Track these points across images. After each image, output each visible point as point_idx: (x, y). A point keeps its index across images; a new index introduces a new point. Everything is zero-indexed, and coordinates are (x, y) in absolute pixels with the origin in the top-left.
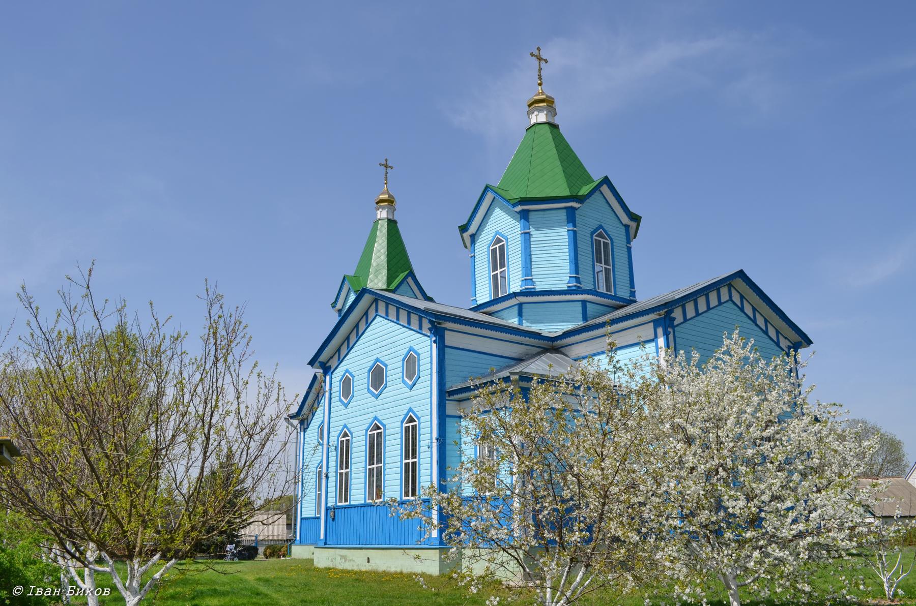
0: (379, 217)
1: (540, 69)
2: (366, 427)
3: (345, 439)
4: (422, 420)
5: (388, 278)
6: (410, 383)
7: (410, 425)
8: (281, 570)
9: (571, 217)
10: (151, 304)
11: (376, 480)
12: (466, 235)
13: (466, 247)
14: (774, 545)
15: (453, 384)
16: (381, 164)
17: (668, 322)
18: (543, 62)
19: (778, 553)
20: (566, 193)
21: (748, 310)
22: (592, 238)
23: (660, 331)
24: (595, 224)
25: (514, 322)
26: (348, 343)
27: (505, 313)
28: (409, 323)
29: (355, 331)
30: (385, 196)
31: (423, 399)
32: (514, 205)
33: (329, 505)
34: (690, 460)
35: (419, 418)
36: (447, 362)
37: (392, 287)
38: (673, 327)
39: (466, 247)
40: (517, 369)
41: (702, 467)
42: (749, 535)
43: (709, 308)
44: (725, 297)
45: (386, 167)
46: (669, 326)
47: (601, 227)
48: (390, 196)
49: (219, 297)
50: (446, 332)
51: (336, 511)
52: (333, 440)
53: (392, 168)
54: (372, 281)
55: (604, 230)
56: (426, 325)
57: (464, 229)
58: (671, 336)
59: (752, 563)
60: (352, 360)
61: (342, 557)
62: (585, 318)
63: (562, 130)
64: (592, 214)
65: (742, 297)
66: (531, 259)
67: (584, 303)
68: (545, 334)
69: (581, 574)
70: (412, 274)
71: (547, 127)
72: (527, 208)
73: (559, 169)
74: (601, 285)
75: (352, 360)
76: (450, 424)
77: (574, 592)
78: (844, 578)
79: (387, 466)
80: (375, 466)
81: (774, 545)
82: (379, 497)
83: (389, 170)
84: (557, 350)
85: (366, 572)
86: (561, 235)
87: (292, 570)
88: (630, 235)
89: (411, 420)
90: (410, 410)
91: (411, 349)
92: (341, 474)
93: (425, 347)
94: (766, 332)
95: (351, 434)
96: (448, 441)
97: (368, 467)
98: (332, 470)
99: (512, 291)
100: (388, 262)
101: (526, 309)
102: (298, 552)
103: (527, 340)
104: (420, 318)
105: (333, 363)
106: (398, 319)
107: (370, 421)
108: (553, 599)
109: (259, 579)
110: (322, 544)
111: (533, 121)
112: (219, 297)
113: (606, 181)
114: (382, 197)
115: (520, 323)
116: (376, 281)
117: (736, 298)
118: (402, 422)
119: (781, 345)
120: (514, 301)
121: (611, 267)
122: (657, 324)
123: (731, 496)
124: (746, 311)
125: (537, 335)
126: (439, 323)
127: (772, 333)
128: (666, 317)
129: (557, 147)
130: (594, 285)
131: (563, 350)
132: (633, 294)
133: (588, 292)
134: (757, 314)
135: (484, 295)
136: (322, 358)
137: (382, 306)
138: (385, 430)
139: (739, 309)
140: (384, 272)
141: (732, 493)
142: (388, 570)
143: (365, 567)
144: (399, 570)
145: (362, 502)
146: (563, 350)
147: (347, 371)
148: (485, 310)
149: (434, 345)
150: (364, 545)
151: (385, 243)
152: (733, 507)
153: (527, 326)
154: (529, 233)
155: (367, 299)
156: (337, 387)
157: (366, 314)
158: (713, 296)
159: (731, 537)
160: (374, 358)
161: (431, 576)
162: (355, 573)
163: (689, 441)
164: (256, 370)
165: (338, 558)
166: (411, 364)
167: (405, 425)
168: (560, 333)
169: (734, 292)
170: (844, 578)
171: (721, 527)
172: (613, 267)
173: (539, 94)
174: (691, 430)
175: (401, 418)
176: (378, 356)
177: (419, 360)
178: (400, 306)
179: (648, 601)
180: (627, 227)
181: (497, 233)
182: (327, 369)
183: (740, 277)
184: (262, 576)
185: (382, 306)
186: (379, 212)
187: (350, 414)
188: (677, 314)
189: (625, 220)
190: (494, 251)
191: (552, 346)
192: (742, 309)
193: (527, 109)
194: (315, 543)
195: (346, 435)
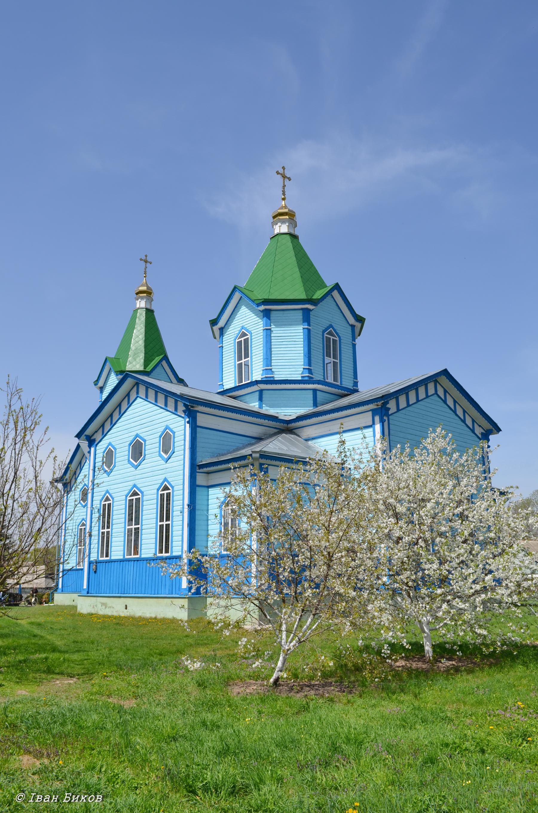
0: (138, 306)
1: (284, 186)
2: (126, 493)
3: (107, 503)
4: (175, 488)
5: (145, 361)
6: (166, 456)
8: (48, 615)
9: (307, 316)
11: (134, 539)
12: (216, 328)
13: (215, 338)
14: (457, 599)
15: (203, 459)
16: (141, 260)
17: (384, 412)
18: (287, 180)
19: (461, 606)
20: (303, 296)
21: (450, 402)
22: (323, 335)
23: (377, 418)
24: (326, 324)
25: (254, 405)
26: (110, 421)
27: (247, 398)
28: (166, 405)
30: (144, 288)
31: (177, 470)
32: (258, 305)
33: (91, 559)
34: (397, 533)
35: (173, 487)
36: (198, 440)
37: (149, 369)
38: (388, 416)
39: (215, 338)
41: (407, 538)
43: (418, 400)
44: (431, 391)
45: (146, 262)
46: (385, 415)
47: (331, 326)
48: (148, 288)
49: (19, 391)
50: (198, 414)
51: (98, 565)
52: (96, 503)
53: (151, 263)
54: (130, 363)
55: (333, 328)
56: (181, 407)
57: (214, 323)
58: (386, 424)
59: (441, 613)
60: (115, 435)
61: (103, 604)
62: (315, 404)
63: (301, 240)
64: (324, 315)
65: (445, 391)
66: (271, 351)
67: (315, 391)
68: (281, 417)
69: (310, 620)
70: (166, 358)
71: (288, 237)
73: (298, 275)
75: (115, 435)
77: (303, 636)
78: (511, 624)
79: (144, 527)
80: (133, 527)
81: (457, 599)
82: (167, 551)
83: (148, 264)
84: (290, 431)
85: (125, 617)
87: (59, 615)
88: (355, 333)
90: (166, 480)
91: (167, 428)
92: (103, 533)
93: (180, 427)
94: (464, 421)
95: (113, 498)
96: (197, 507)
97: (127, 527)
100: (146, 347)
101: (265, 394)
102: (60, 599)
103: (266, 422)
106: (156, 401)
107: (130, 487)
108: (287, 640)
109: (32, 623)
110: (85, 593)
111: (277, 231)
112: (19, 391)
113: (337, 287)
114: (142, 288)
115: (261, 407)
116: (134, 363)
117: (441, 392)
118: (158, 490)
119: (476, 432)
120: (256, 388)
121: (338, 361)
122: (374, 412)
123: (428, 560)
124: (448, 403)
125: (274, 418)
126: (192, 407)
127: (469, 422)
128: (382, 407)
129: (296, 255)
130: (324, 376)
132: (356, 384)
133: (318, 382)
135: (230, 382)
136: (88, 432)
138: (143, 496)
140: (142, 356)
141: (430, 557)
142: (143, 615)
143: (124, 613)
144: (153, 616)
145: (122, 557)
147: (110, 444)
148: (230, 394)
149: (188, 425)
150: (122, 593)
151: (143, 330)
152: (428, 570)
154: (270, 329)
155: (129, 382)
157: (128, 395)
158: (422, 390)
159: (426, 593)
160: (135, 433)
162: (115, 618)
163: (397, 516)
164: (53, 455)
165: (99, 605)
166: (167, 442)
167: (160, 493)
168: (293, 417)
169: (439, 387)
170: (511, 624)
171: (418, 585)
172: (340, 361)
173: (282, 208)
174: (401, 509)
175: (157, 486)
176: (138, 432)
177: (174, 437)
178: (158, 390)
179: (361, 641)
180: (353, 326)
181: (243, 328)
182: (91, 442)
183: (444, 375)
184: (33, 620)
186: (138, 302)
187: (116, 483)
188: (392, 405)
189: (352, 320)
190: (240, 343)
191: (287, 427)
192: (445, 402)
193: (272, 220)
194: (77, 590)
195: (107, 499)
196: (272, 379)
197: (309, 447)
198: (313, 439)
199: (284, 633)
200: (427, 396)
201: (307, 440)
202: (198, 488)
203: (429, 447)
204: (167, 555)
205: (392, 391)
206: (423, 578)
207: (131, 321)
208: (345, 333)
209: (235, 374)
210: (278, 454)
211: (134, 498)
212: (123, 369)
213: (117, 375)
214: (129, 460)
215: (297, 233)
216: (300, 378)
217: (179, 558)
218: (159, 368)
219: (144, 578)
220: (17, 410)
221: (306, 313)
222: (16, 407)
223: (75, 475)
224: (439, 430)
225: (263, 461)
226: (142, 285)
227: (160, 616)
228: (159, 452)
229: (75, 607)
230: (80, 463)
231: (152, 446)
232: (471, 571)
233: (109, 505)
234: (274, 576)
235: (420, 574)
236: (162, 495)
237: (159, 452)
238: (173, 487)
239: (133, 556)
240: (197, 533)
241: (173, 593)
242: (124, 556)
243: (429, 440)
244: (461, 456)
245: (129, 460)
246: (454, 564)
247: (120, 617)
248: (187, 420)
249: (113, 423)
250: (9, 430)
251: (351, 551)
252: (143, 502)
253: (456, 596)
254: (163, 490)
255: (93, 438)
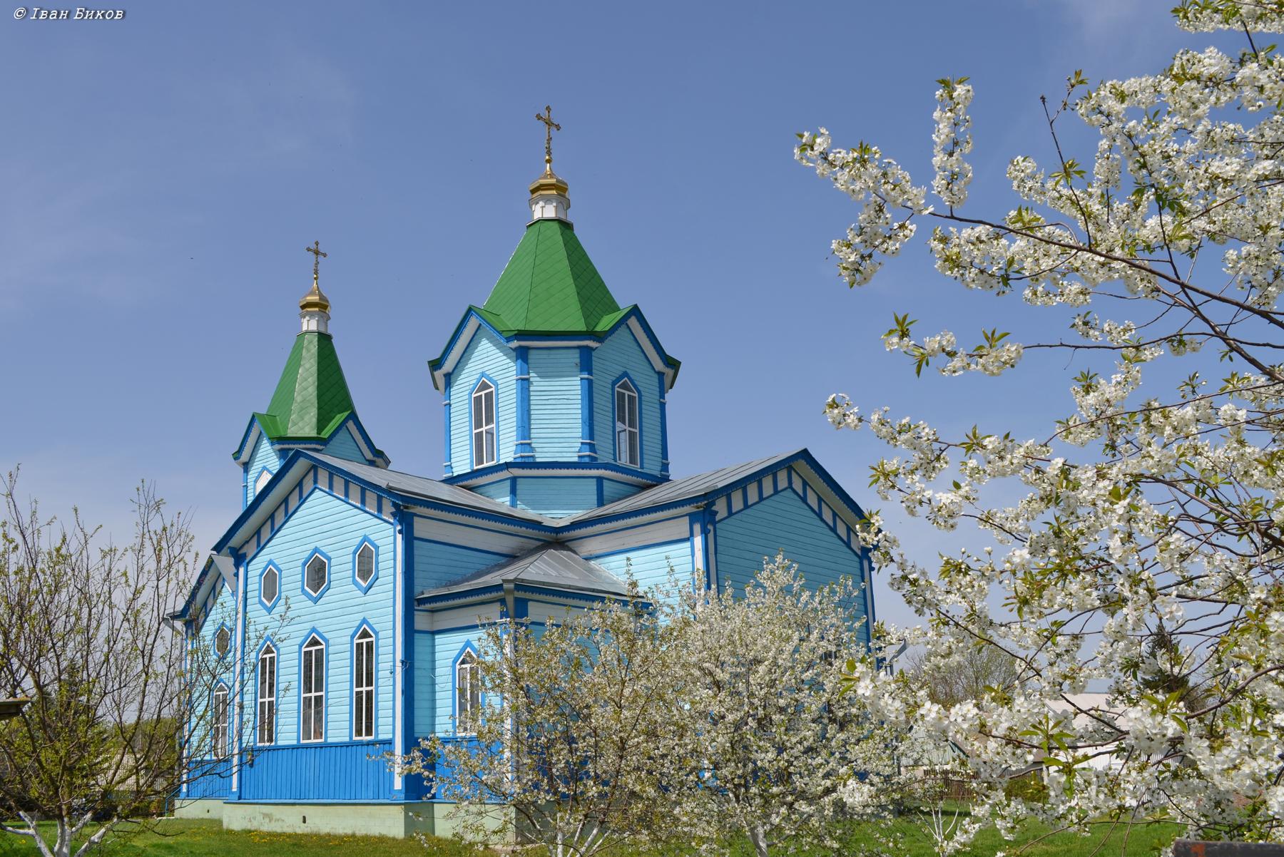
0: (305, 328)
5: (319, 421)
6: (364, 585)
7: (364, 641)
9: (586, 364)
10: (76, 510)
11: (314, 710)
12: (439, 374)
13: (437, 388)
16: (309, 249)
20: (581, 326)
21: (812, 500)
22: (613, 389)
23: (697, 528)
24: (618, 371)
25: (502, 502)
29: (283, 507)
30: (315, 298)
31: (383, 606)
32: (508, 340)
35: (376, 633)
36: (416, 559)
37: (326, 434)
38: (714, 523)
39: (437, 388)
40: (511, 573)
42: (775, 790)
43: (761, 499)
44: (783, 483)
45: (317, 253)
47: (625, 374)
50: (416, 519)
53: (325, 255)
54: (295, 424)
56: (388, 507)
57: (435, 365)
58: (711, 536)
61: (265, 815)
62: (601, 503)
64: (612, 358)
65: (805, 484)
66: (529, 415)
67: (600, 480)
69: (595, 832)
70: (353, 416)
71: (556, 226)
72: (526, 344)
73: (571, 290)
74: (623, 456)
76: (420, 642)
82: (369, 733)
83: (321, 258)
86: (573, 386)
89: (365, 634)
90: (364, 621)
91: (365, 539)
93: (387, 539)
96: (416, 665)
98: (248, 699)
99: (502, 462)
100: (319, 397)
104: (380, 499)
105: (250, 550)
113: (635, 311)
115: (513, 505)
116: (301, 424)
118: (352, 637)
120: (505, 474)
122: (693, 518)
123: (759, 747)
125: (536, 525)
126: (406, 508)
128: (704, 511)
129: (569, 256)
130: (614, 454)
131: (570, 544)
132: (665, 467)
133: (606, 466)
134: (823, 505)
135: (462, 463)
136: (234, 542)
137: (323, 475)
138: (327, 646)
139: (795, 511)
142: (332, 832)
143: (301, 829)
144: (349, 832)
145: (295, 742)
146: (570, 544)
147: (271, 562)
148: (465, 483)
149: (399, 537)
150: (297, 798)
151: (315, 368)
153: (524, 511)
154: (527, 379)
156: (255, 584)
157: (300, 484)
160: (312, 546)
161: (394, 839)
162: (289, 836)
166: (365, 563)
167: (356, 641)
169: (794, 476)
172: (641, 430)
174: (722, 676)
175: (351, 631)
176: (318, 544)
177: (377, 555)
178: (349, 478)
181: (483, 375)
182: (240, 559)
185: (323, 475)
186: (305, 321)
188: (720, 507)
189: (659, 365)
190: (478, 399)
191: (557, 539)
192: (804, 499)
196: (531, 460)
197: (591, 570)
198: (598, 557)
199: (560, 848)
200: (776, 492)
201: (587, 559)
202: (417, 636)
203: (767, 584)
204: (369, 738)
205: (720, 485)
206: (754, 772)
207: (293, 353)
208: (648, 383)
209: (471, 449)
210: (544, 583)
211: (313, 649)
212: (282, 434)
213: (272, 444)
214: (303, 589)
215: (570, 219)
216: (576, 459)
217: (390, 742)
218: (342, 435)
219: (332, 774)
220: (159, 532)
221: (586, 353)
222: (156, 525)
223: (205, 609)
224: (779, 558)
225: (520, 595)
226: (312, 293)
227: (361, 832)
228: (354, 577)
229: (220, 822)
230: (214, 588)
231: (342, 567)
232: (819, 760)
233: (272, 659)
234: (544, 768)
235: (750, 765)
236: (308, 654)
237: (354, 577)
238: (376, 633)
239: (313, 741)
240: (416, 704)
241: (380, 798)
242: (299, 740)
243: (765, 574)
244: (812, 597)
245: (303, 589)
246: (795, 752)
247: (296, 835)
248: (399, 528)
249: (276, 528)
250: (145, 559)
251: (652, 734)
252: (328, 655)
253: (802, 795)
254: (360, 638)
255: (241, 552)
